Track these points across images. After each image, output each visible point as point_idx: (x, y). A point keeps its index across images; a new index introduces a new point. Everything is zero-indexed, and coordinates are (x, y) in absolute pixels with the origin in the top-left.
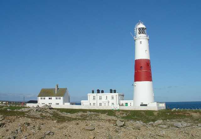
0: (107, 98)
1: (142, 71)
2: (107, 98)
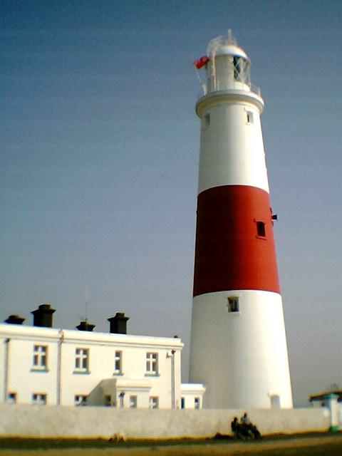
0: (118, 365)
1: (228, 246)
2: (118, 365)
